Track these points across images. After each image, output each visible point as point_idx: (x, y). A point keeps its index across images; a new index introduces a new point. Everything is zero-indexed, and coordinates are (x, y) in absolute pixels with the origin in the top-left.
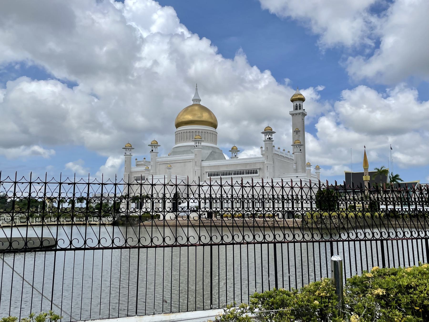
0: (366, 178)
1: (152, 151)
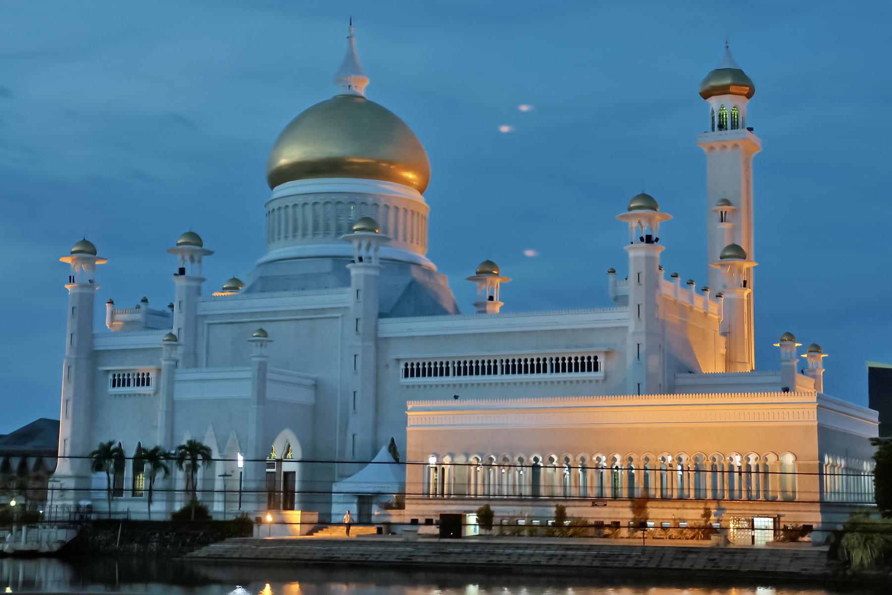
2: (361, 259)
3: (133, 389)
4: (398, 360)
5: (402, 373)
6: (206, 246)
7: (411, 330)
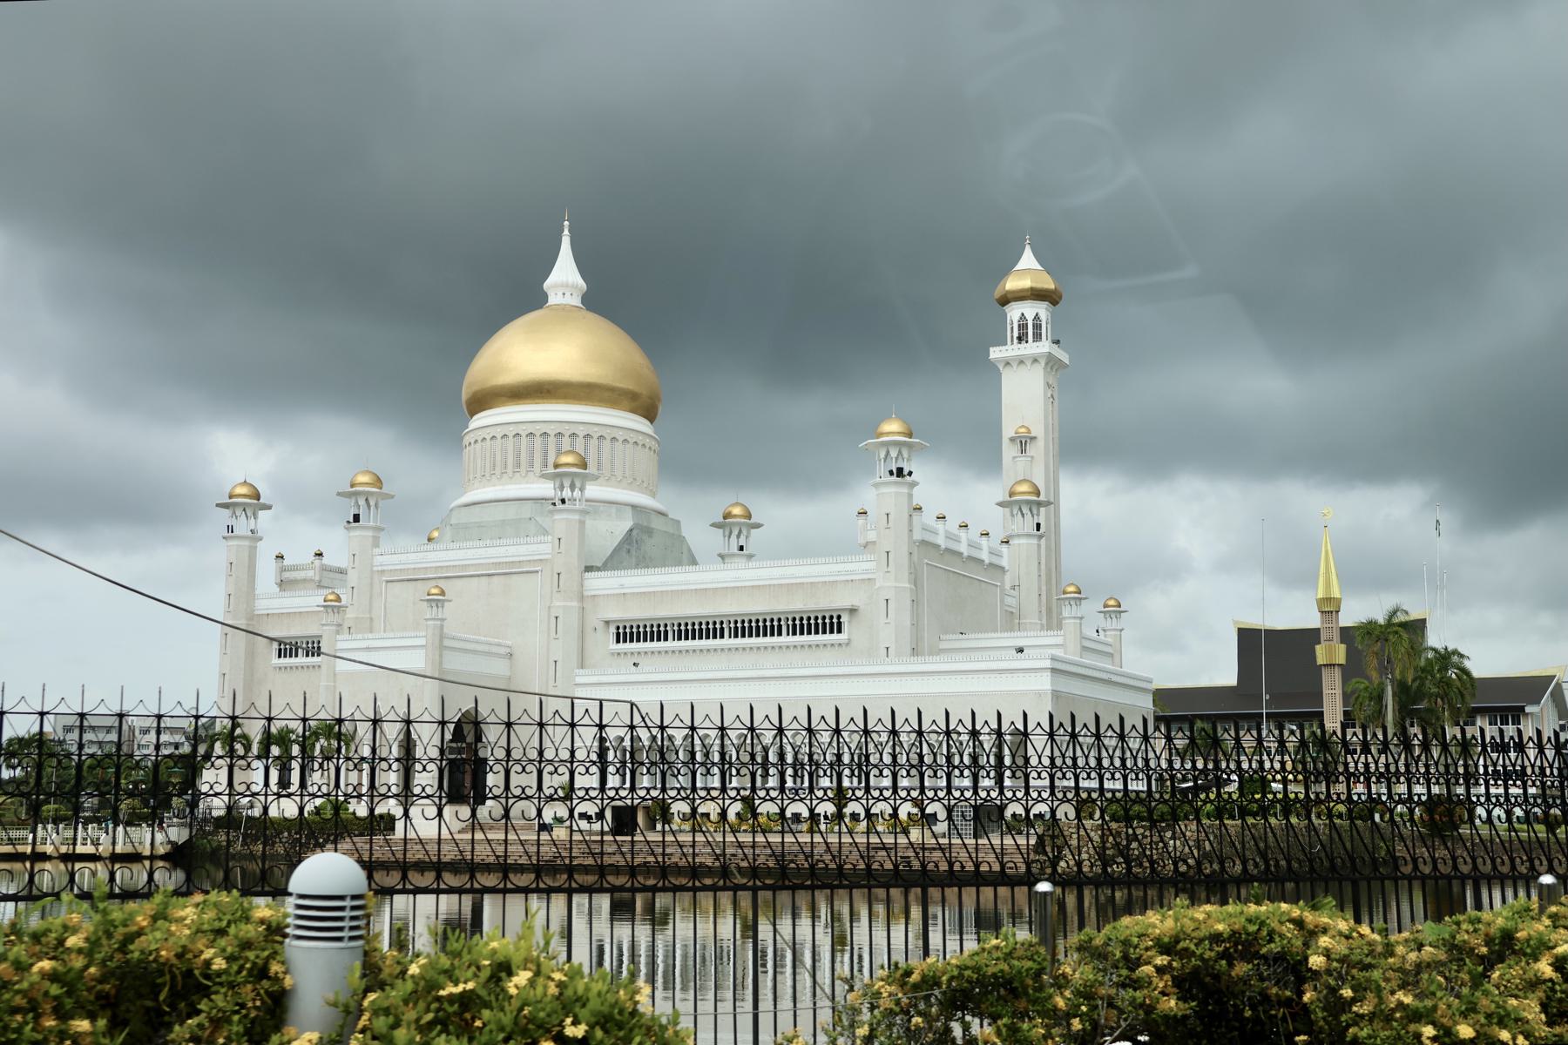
0: (1330, 652)
1: (230, 529)
2: (563, 501)
3: (302, 660)
4: (607, 623)
5: (612, 638)
6: (384, 490)
7: (622, 586)
